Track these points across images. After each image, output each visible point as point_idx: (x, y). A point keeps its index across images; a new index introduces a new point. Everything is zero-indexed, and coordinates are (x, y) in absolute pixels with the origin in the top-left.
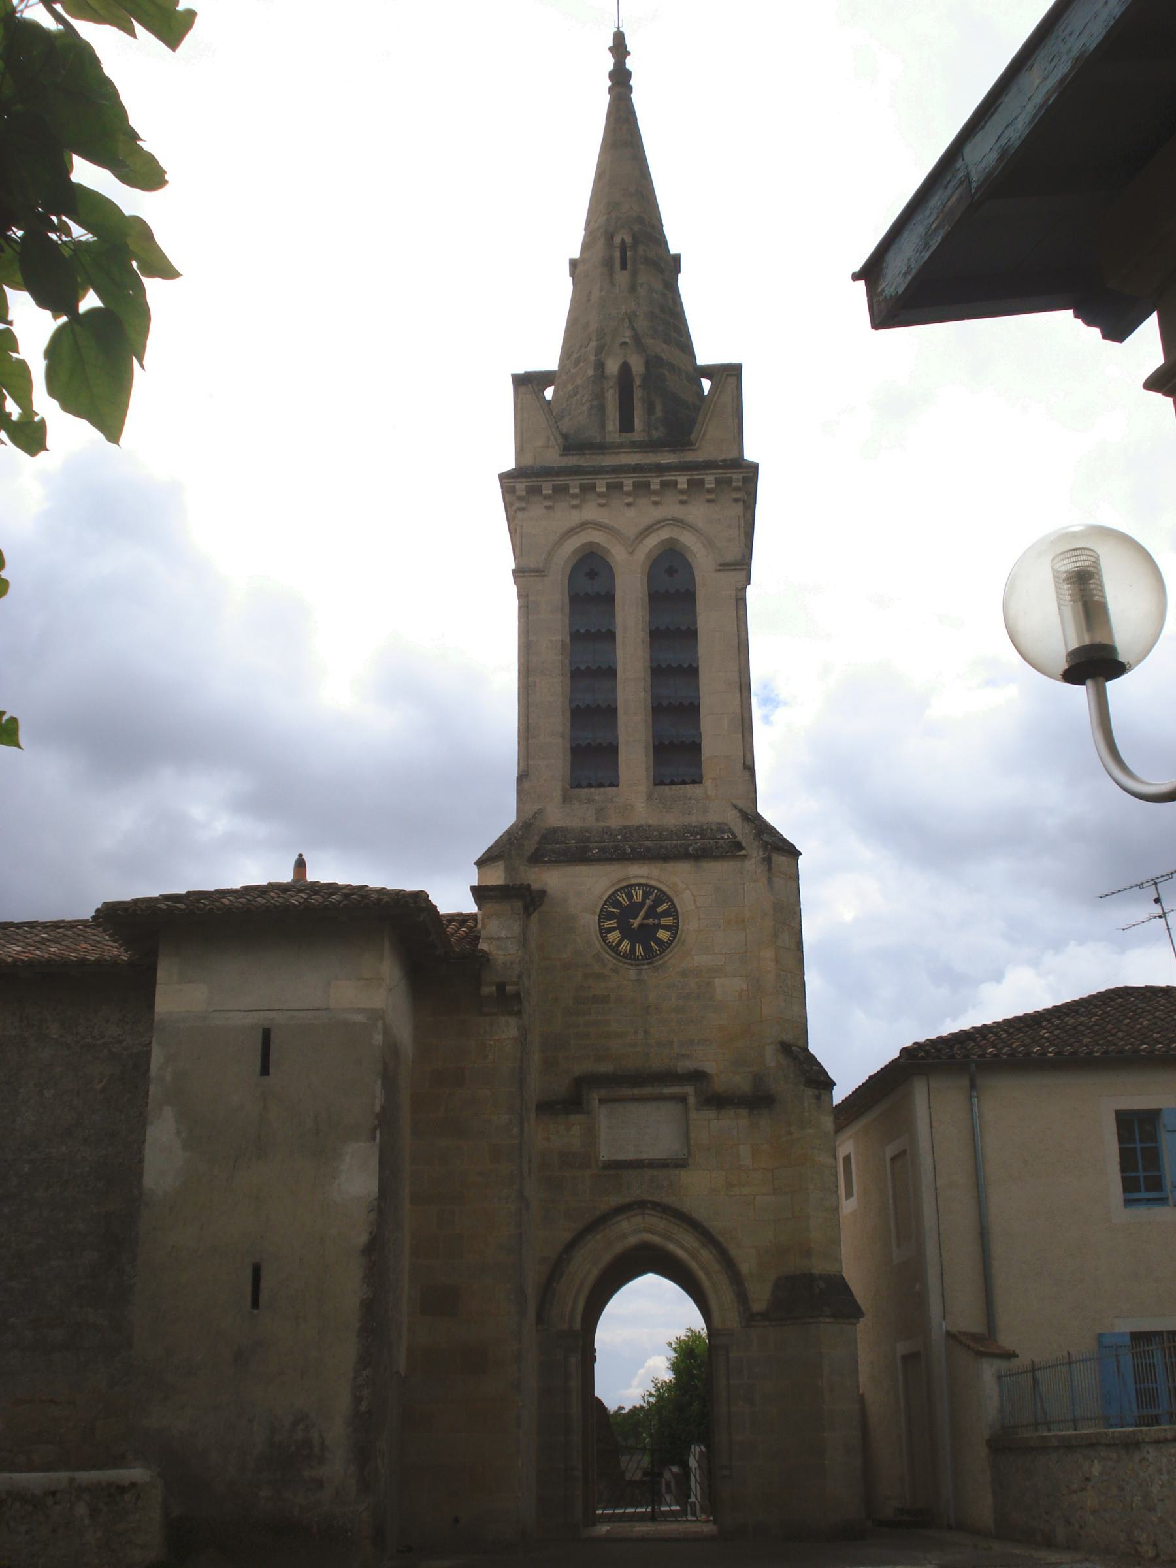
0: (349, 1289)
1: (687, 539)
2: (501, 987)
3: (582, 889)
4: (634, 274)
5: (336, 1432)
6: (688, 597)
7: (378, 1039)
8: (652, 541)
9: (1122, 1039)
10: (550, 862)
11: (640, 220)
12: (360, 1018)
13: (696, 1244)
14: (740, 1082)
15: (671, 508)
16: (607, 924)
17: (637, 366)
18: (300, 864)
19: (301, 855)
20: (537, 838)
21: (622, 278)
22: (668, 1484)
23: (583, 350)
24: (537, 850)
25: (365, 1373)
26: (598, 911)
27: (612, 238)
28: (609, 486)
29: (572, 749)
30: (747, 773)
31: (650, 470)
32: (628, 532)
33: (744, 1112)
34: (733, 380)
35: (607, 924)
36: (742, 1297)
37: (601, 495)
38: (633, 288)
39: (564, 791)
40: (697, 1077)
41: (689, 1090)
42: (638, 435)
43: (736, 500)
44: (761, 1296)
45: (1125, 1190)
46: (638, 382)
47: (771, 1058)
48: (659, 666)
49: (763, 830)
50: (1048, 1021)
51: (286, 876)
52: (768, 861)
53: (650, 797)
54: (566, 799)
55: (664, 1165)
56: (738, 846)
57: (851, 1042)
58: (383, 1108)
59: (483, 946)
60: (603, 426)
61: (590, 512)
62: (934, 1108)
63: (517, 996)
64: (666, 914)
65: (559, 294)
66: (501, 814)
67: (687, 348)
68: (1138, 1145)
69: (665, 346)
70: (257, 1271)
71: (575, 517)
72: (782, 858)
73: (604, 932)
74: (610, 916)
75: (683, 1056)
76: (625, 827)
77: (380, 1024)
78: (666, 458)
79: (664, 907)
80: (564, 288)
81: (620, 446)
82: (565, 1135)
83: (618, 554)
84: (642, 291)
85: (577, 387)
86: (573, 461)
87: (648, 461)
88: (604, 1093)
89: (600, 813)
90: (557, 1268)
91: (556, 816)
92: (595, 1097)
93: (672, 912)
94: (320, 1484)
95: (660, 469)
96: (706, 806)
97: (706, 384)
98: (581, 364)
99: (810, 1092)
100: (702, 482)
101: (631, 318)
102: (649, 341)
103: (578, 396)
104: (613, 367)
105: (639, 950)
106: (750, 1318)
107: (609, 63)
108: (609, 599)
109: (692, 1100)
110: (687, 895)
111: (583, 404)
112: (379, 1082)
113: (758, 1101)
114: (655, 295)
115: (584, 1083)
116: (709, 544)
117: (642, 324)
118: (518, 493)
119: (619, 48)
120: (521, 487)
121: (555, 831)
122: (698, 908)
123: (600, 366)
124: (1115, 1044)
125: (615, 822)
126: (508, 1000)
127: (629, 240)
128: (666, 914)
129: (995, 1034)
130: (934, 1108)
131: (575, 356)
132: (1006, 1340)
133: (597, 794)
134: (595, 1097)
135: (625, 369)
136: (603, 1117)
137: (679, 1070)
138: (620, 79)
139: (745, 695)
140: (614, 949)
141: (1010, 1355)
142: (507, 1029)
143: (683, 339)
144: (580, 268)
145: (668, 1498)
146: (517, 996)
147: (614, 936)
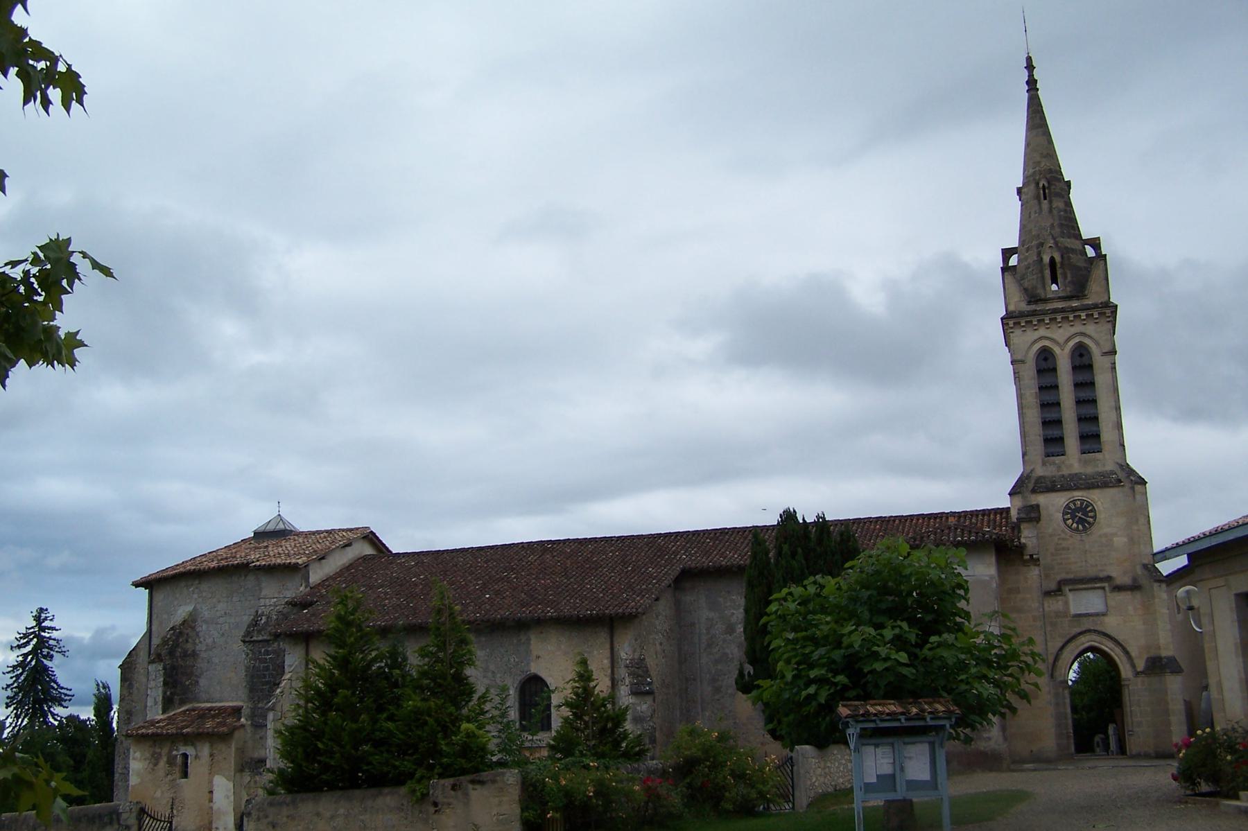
1: (1087, 341)
3: (1053, 504)
4: (1050, 202)
8: (1072, 343)
15: (1078, 328)
17: (1058, 258)
21: (1045, 204)
32: (1061, 338)
36: (1133, 666)
40: (1109, 579)
41: (1106, 585)
44: (1141, 666)
47: (1139, 571)
49: (1131, 472)
52: (1133, 489)
53: (1080, 460)
54: (1044, 464)
55: (1097, 615)
56: (1120, 481)
59: (1023, 540)
61: (1042, 332)
65: (1012, 210)
73: (1065, 520)
78: (1075, 304)
80: (1017, 204)
82: (1054, 605)
83: (1057, 350)
84: (1055, 212)
86: (1033, 307)
91: (1040, 471)
92: (1066, 589)
93: (1093, 510)
94: (989, 739)
95: (1074, 310)
96: (1105, 462)
99: (1156, 585)
104: (1046, 259)
106: (1137, 674)
113: (1134, 587)
115: (1061, 584)
116: (1097, 344)
119: (1030, 67)
120: (1011, 323)
121: (1041, 477)
123: (1039, 254)
125: (1065, 472)
126: (1034, 561)
133: (1057, 459)
135: (1052, 260)
136: (1071, 596)
138: (1032, 84)
142: (1034, 573)
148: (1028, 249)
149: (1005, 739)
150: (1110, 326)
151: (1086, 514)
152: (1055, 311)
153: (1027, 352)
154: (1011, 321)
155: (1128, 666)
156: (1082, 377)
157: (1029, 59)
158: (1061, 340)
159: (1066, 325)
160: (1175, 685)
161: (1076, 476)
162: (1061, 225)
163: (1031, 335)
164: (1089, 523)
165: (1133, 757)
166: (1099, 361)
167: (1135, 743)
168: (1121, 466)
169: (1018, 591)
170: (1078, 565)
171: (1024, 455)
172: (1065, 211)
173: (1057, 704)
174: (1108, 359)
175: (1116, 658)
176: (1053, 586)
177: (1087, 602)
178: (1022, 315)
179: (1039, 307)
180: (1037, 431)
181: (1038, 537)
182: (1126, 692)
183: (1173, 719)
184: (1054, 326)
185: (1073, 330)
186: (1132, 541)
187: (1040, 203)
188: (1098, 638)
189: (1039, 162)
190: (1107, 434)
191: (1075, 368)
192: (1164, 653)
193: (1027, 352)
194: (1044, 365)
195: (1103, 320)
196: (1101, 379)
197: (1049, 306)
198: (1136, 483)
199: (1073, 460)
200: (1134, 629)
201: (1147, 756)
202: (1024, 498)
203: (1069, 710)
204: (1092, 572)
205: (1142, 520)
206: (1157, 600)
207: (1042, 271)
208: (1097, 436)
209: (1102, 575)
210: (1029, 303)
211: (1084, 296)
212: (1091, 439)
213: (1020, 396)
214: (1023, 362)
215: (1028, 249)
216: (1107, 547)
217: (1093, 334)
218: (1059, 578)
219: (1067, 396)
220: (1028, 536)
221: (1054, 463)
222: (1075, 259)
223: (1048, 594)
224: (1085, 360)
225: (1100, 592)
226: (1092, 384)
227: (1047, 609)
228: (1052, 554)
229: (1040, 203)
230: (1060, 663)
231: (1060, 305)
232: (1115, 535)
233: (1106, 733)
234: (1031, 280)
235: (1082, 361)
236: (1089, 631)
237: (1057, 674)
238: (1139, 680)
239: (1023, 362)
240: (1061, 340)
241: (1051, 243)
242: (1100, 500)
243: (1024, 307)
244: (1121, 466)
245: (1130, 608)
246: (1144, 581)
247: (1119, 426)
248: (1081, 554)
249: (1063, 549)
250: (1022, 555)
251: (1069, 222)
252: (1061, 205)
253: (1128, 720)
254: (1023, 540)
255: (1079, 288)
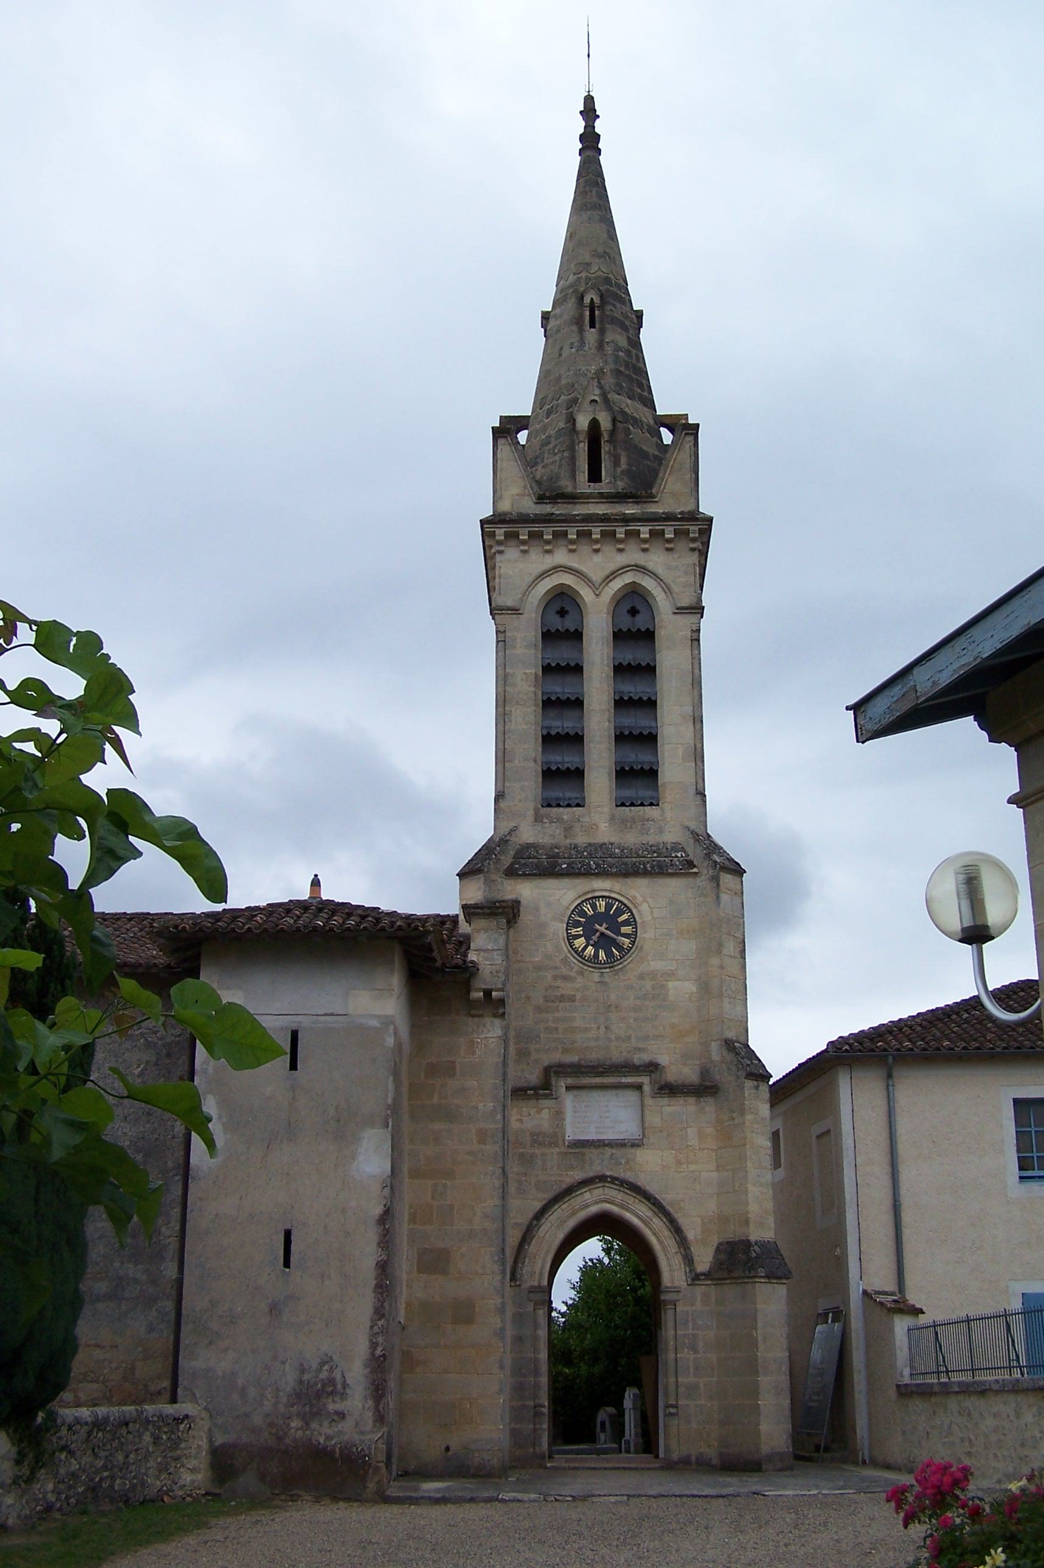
0: (366, 1253)
1: (648, 583)
2: (488, 993)
3: (550, 901)
4: (602, 332)
5: (355, 1373)
6: (648, 636)
7: (390, 1041)
8: (617, 584)
9: (1021, 1035)
10: (524, 875)
11: (607, 281)
12: (375, 1023)
13: (649, 1214)
14: (689, 1073)
15: (633, 555)
16: (573, 931)
17: (605, 423)
18: (316, 883)
19: (316, 876)
20: (512, 853)
21: (591, 335)
22: (603, 1424)
23: (555, 402)
24: (512, 864)
25: (380, 1323)
26: (566, 920)
27: (582, 298)
28: (579, 534)
29: (543, 771)
30: (699, 797)
31: (616, 520)
32: (596, 574)
33: (692, 1100)
34: (691, 438)
35: (573, 931)
36: (689, 1260)
37: (572, 542)
38: (601, 346)
39: (536, 811)
40: (652, 1068)
41: (645, 1080)
42: (604, 487)
43: (693, 550)
44: (704, 1260)
45: (1021, 1169)
46: (606, 436)
47: (716, 1052)
48: (621, 698)
49: (712, 848)
50: (957, 1014)
51: (304, 894)
52: (716, 879)
53: (612, 818)
54: (538, 819)
55: (621, 1144)
56: (691, 864)
57: (783, 1039)
58: (394, 1099)
59: (472, 956)
60: (573, 476)
61: (561, 557)
62: (857, 1101)
63: (502, 1002)
64: (626, 923)
65: (531, 348)
66: (478, 827)
67: (650, 403)
68: (1033, 1129)
69: (629, 401)
70: (288, 1234)
71: (549, 561)
72: (729, 876)
73: (571, 938)
74: (577, 924)
75: (639, 1049)
76: (590, 844)
77: (391, 1030)
78: (630, 510)
79: (625, 917)
80: (538, 340)
81: (589, 496)
82: (531, 1118)
83: (586, 594)
84: (609, 350)
85: (549, 437)
86: (547, 509)
87: (614, 512)
88: (570, 1081)
89: (568, 830)
90: (528, 1234)
91: (528, 834)
92: (561, 1084)
93: (632, 922)
94: (342, 1415)
95: (626, 520)
96: (665, 826)
97: (667, 437)
98: (553, 416)
99: (749, 1084)
100: (663, 532)
101: (599, 374)
102: (613, 397)
103: (551, 446)
104: (583, 422)
105: (602, 954)
106: (696, 1278)
107: (580, 126)
108: (577, 636)
109: (647, 1088)
110: (644, 907)
111: (555, 454)
112: (391, 1078)
113: (704, 1089)
114: (620, 353)
115: (552, 1072)
116: (667, 589)
117: (609, 381)
118: (497, 538)
119: (589, 112)
120: (500, 533)
121: (528, 846)
122: (654, 919)
123: (571, 420)
124: (1015, 1040)
125: (581, 840)
126: (493, 1004)
127: (597, 300)
128: (626, 923)
129: (910, 1027)
130: (857, 1101)
131: (547, 407)
132: (913, 1298)
133: (566, 813)
134: (561, 1084)
135: (594, 424)
136: (569, 1101)
137: (636, 1062)
138: (590, 141)
139: (698, 727)
140: (580, 953)
141: (917, 1312)
142: (491, 1031)
143: (642, 365)
144: (552, 323)
145: (602, 1436)
146: (502, 1002)
147: (580, 942)
148: (549, 413)
149: (380, 1418)
150: (691, 438)
151: (615, 927)
152: (589, 519)
153: (526, 593)
154: (500, 530)
155: (678, 1261)
156: (632, 655)
157: (589, 101)
158: (597, 576)
159: (608, 549)
160: (771, 1302)
161: (601, 850)
162: (618, 373)
163: (537, 561)
164: (620, 948)
165: (670, 1466)
166: (669, 627)
167: (678, 1436)
168: (695, 836)
169: (450, 1070)
170: (589, 1033)
171: (499, 797)
172: (628, 353)
173: (519, 1339)
174: (688, 620)
175: (653, 1240)
176: (533, 1077)
177: (602, 1115)
178: (524, 519)
179: (559, 510)
180: (530, 754)
181: (506, 952)
182: (668, 1317)
183: (765, 1381)
184: (585, 549)
185: (621, 560)
186: (705, 988)
187: (581, 330)
188: (619, 1196)
189: (588, 264)
190: (672, 769)
191: (619, 636)
192: (755, 1235)
193: (526, 593)
194: (557, 623)
195: (682, 546)
196: (669, 659)
197: (580, 510)
198: (724, 868)
199: (599, 817)
200: (701, 1179)
201: (702, 1466)
202: (489, 882)
203: (543, 1355)
204: (617, 1054)
205: (730, 948)
206: (749, 1117)
207: (572, 448)
208: (651, 774)
209: (638, 1059)
210: (541, 499)
211: (650, 498)
212: (638, 778)
213: (503, 679)
214: (515, 611)
215: (549, 413)
216: (647, 1004)
217: (660, 571)
218: (547, 1059)
219: (598, 688)
220: (485, 947)
221: (559, 820)
222: (636, 435)
223: (520, 1093)
224: (640, 622)
225: (632, 1096)
226: (650, 670)
227: (514, 1124)
228: (539, 1009)
229: (581, 330)
230: (532, 1248)
231: (601, 509)
232: (671, 975)
233: (618, 1404)
234: (552, 464)
235: (635, 631)
236: (602, 1178)
237: (525, 1270)
238: (699, 1291)
239: (515, 611)
240: (597, 576)
241: (595, 394)
242: (649, 901)
243: (529, 506)
244: (695, 836)
245: (692, 1132)
246: (724, 1077)
247: (698, 756)
248: (599, 1015)
249: (562, 998)
250: (468, 988)
251: (633, 375)
252: (623, 342)
253: (667, 1381)
254: (472, 956)
255: (642, 487)
